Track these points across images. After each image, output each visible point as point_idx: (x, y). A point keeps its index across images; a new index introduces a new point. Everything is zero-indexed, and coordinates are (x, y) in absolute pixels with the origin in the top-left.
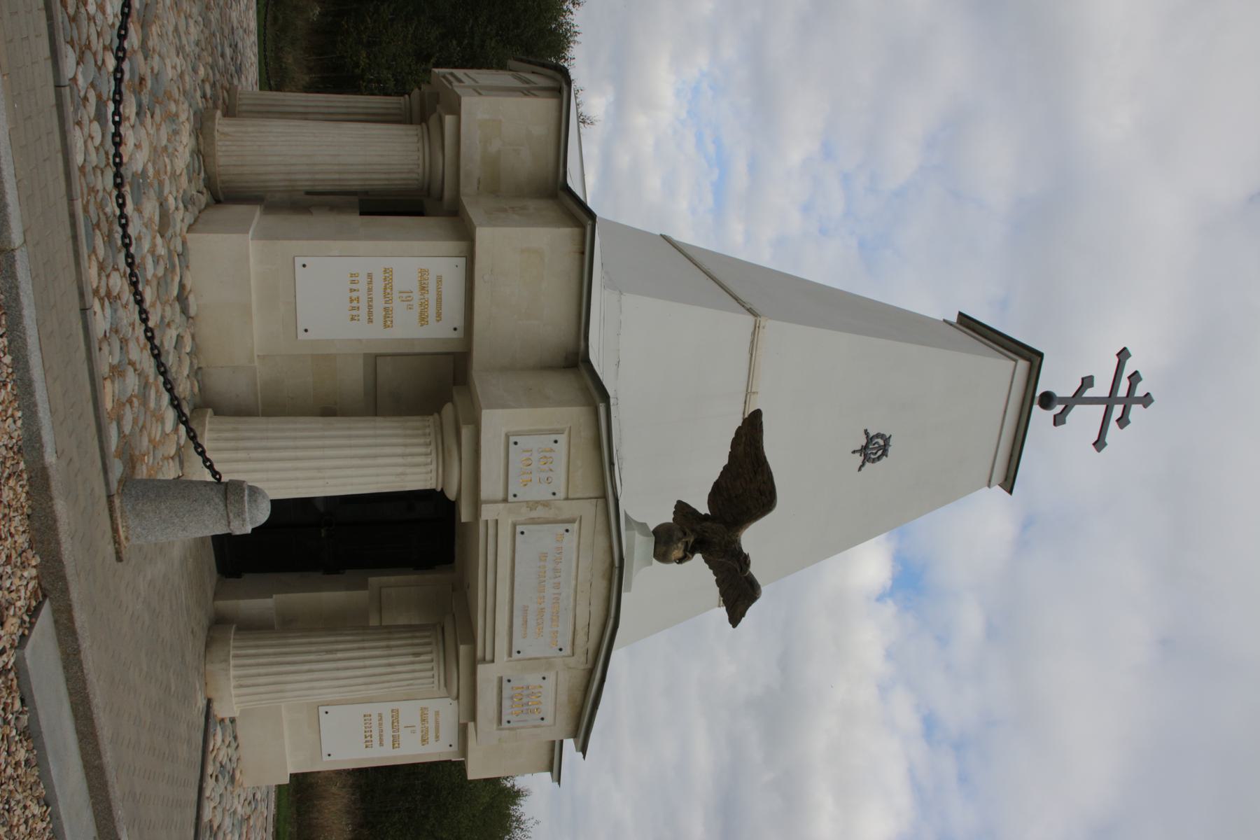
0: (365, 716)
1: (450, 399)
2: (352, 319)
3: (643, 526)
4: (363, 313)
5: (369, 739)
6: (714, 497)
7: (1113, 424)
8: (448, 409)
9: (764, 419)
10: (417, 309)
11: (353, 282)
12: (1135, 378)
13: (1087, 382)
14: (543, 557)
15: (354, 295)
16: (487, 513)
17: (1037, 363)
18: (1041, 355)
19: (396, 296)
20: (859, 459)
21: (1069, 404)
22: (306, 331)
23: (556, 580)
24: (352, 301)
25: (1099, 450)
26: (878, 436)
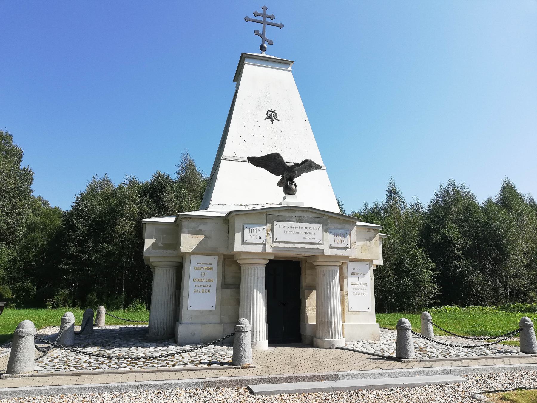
0: (353, 295)
1: (236, 261)
2: (210, 292)
3: (284, 198)
4: (208, 288)
5: (363, 294)
6: (277, 174)
7: (273, 21)
8: (239, 262)
9: (250, 156)
10: (207, 271)
11: (197, 292)
12: (255, 14)
13: (257, 33)
14: (286, 232)
15: (201, 291)
16: (269, 249)
17: (246, 55)
18: (243, 54)
19: (203, 278)
20: (275, 121)
21: (265, 40)
22: (212, 307)
23: (294, 228)
24: (203, 292)
25: (283, 26)
26: (267, 115)
